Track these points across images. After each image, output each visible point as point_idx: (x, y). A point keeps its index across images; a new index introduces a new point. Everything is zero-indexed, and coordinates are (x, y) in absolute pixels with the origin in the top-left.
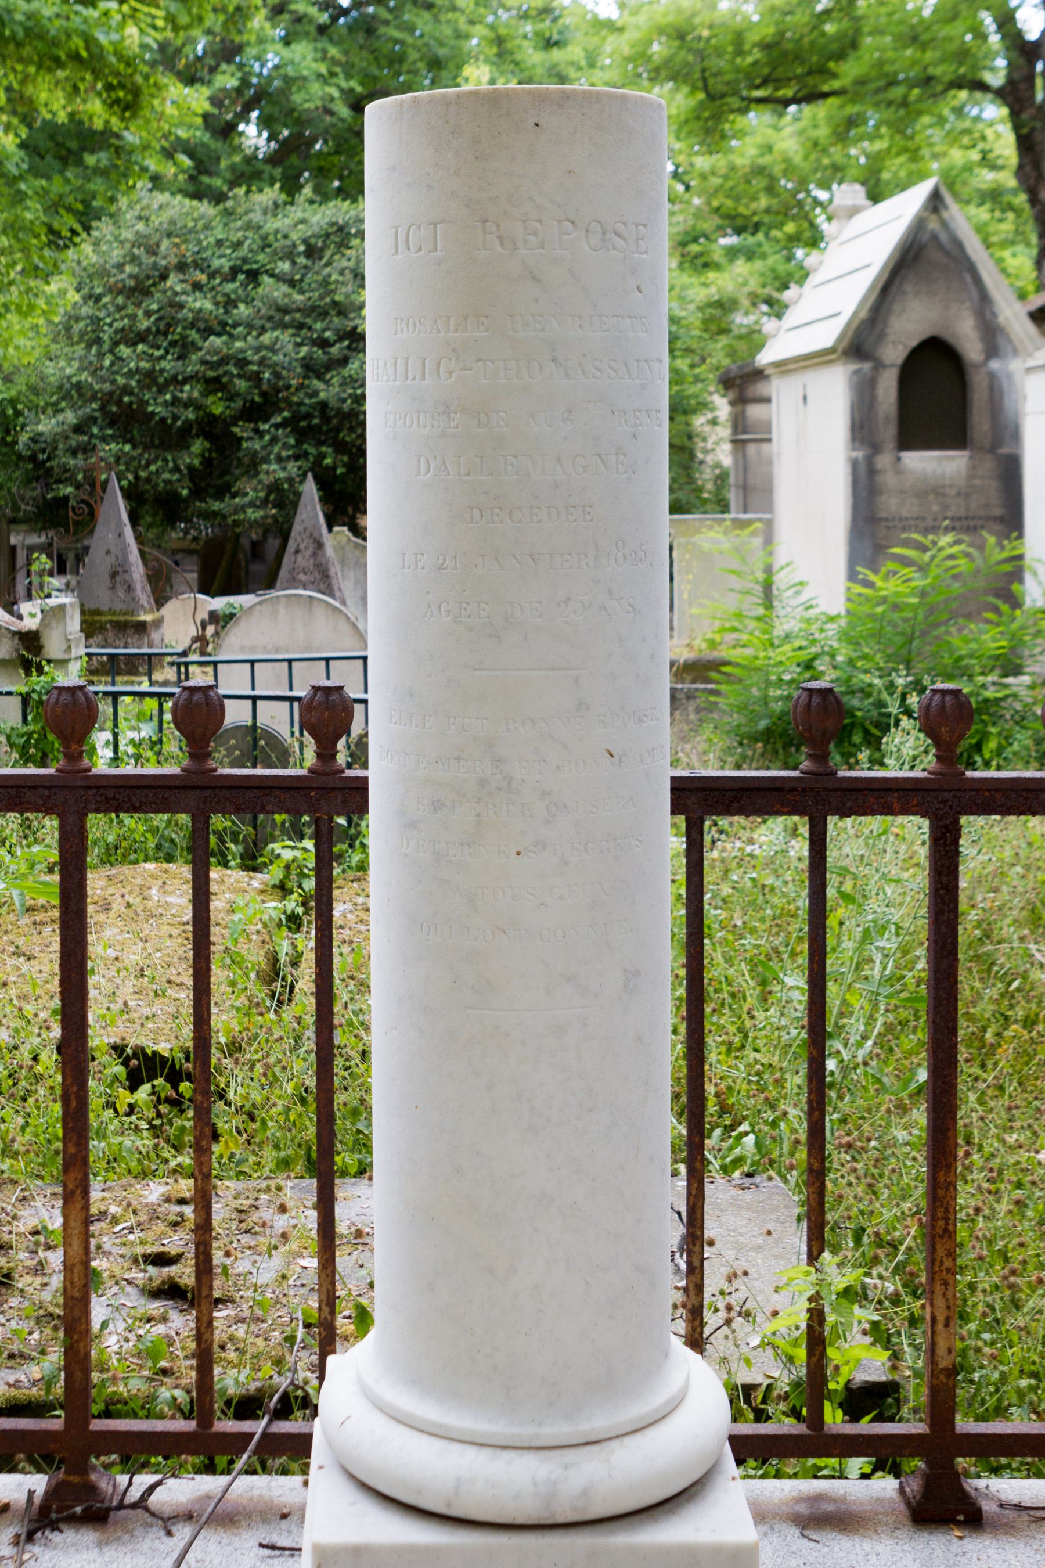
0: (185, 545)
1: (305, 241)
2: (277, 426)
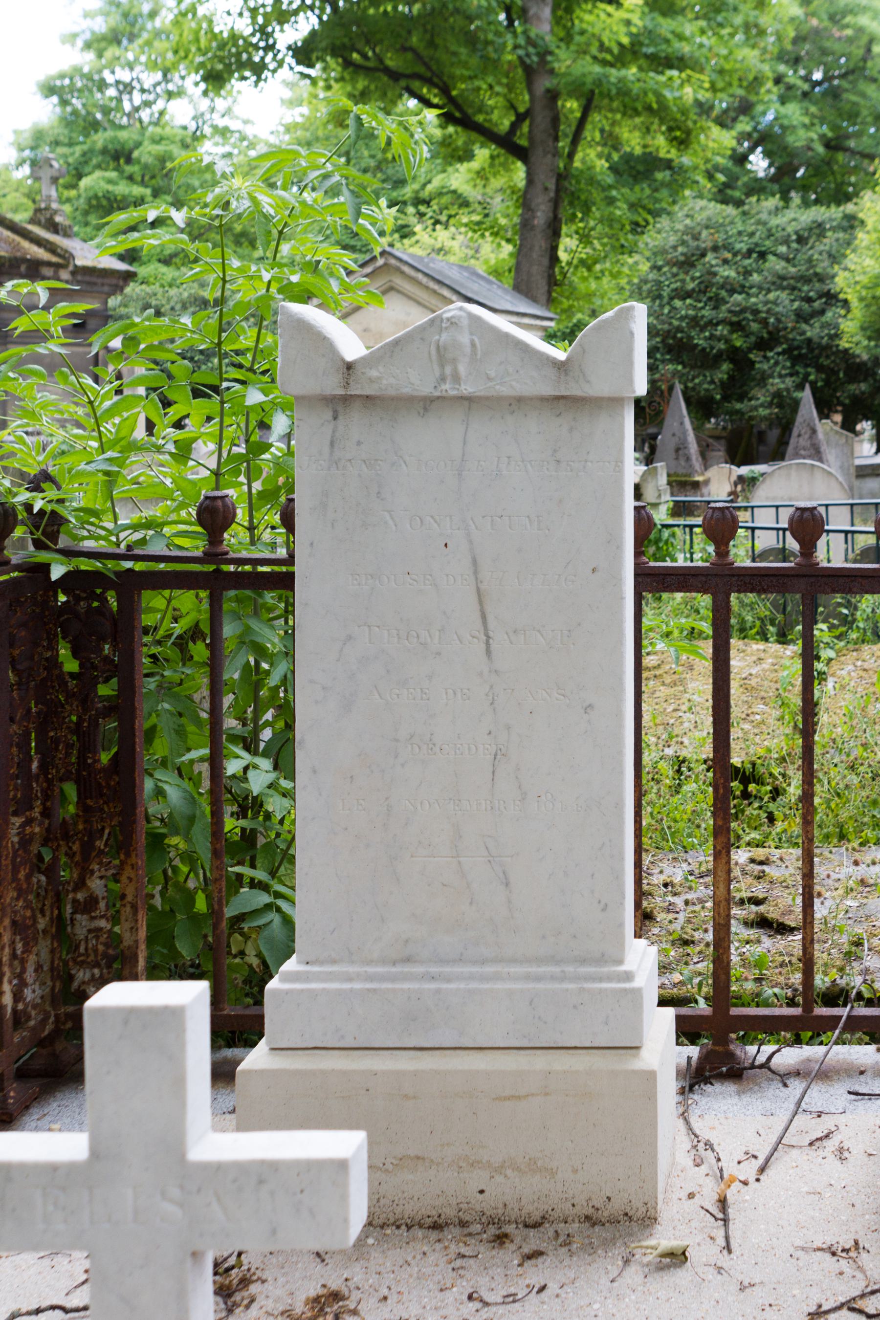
0: (717, 433)
1: (796, 233)
2: (779, 354)
